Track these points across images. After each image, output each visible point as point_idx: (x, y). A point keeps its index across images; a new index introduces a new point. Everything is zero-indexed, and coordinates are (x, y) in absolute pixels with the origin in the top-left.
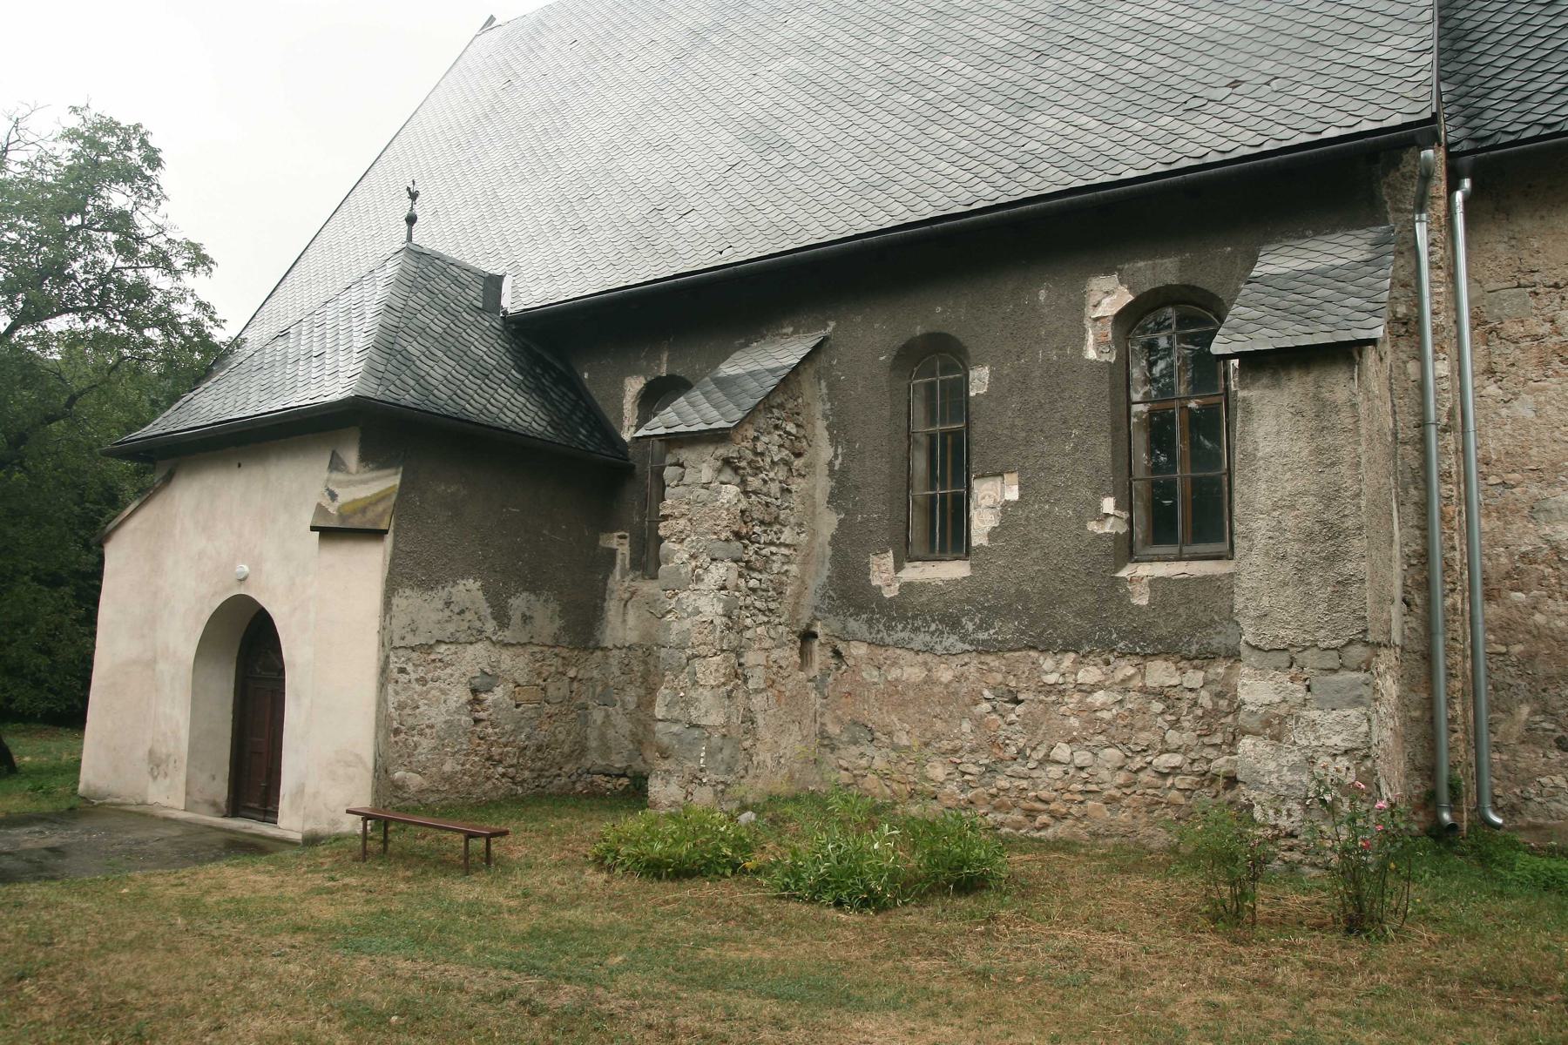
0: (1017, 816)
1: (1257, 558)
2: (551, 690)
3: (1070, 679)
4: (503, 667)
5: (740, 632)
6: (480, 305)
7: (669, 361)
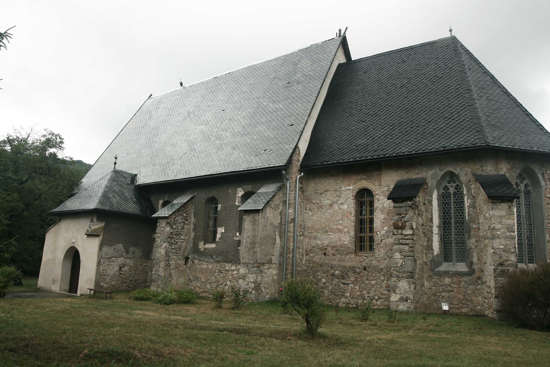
1: (243, 247)
4: (127, 263)
6: (129, 183)
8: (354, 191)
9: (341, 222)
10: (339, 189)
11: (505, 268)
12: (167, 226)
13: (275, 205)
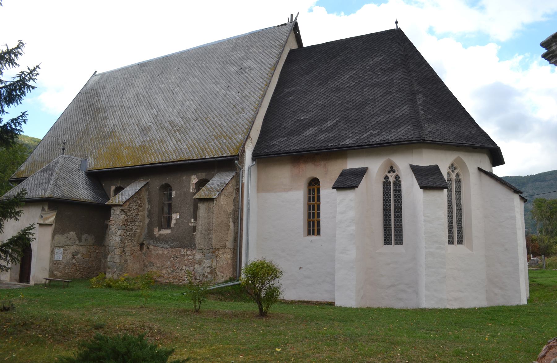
0: (177, 280)
2: (92, 255)
3: (186, 253)
7: (120, 183)
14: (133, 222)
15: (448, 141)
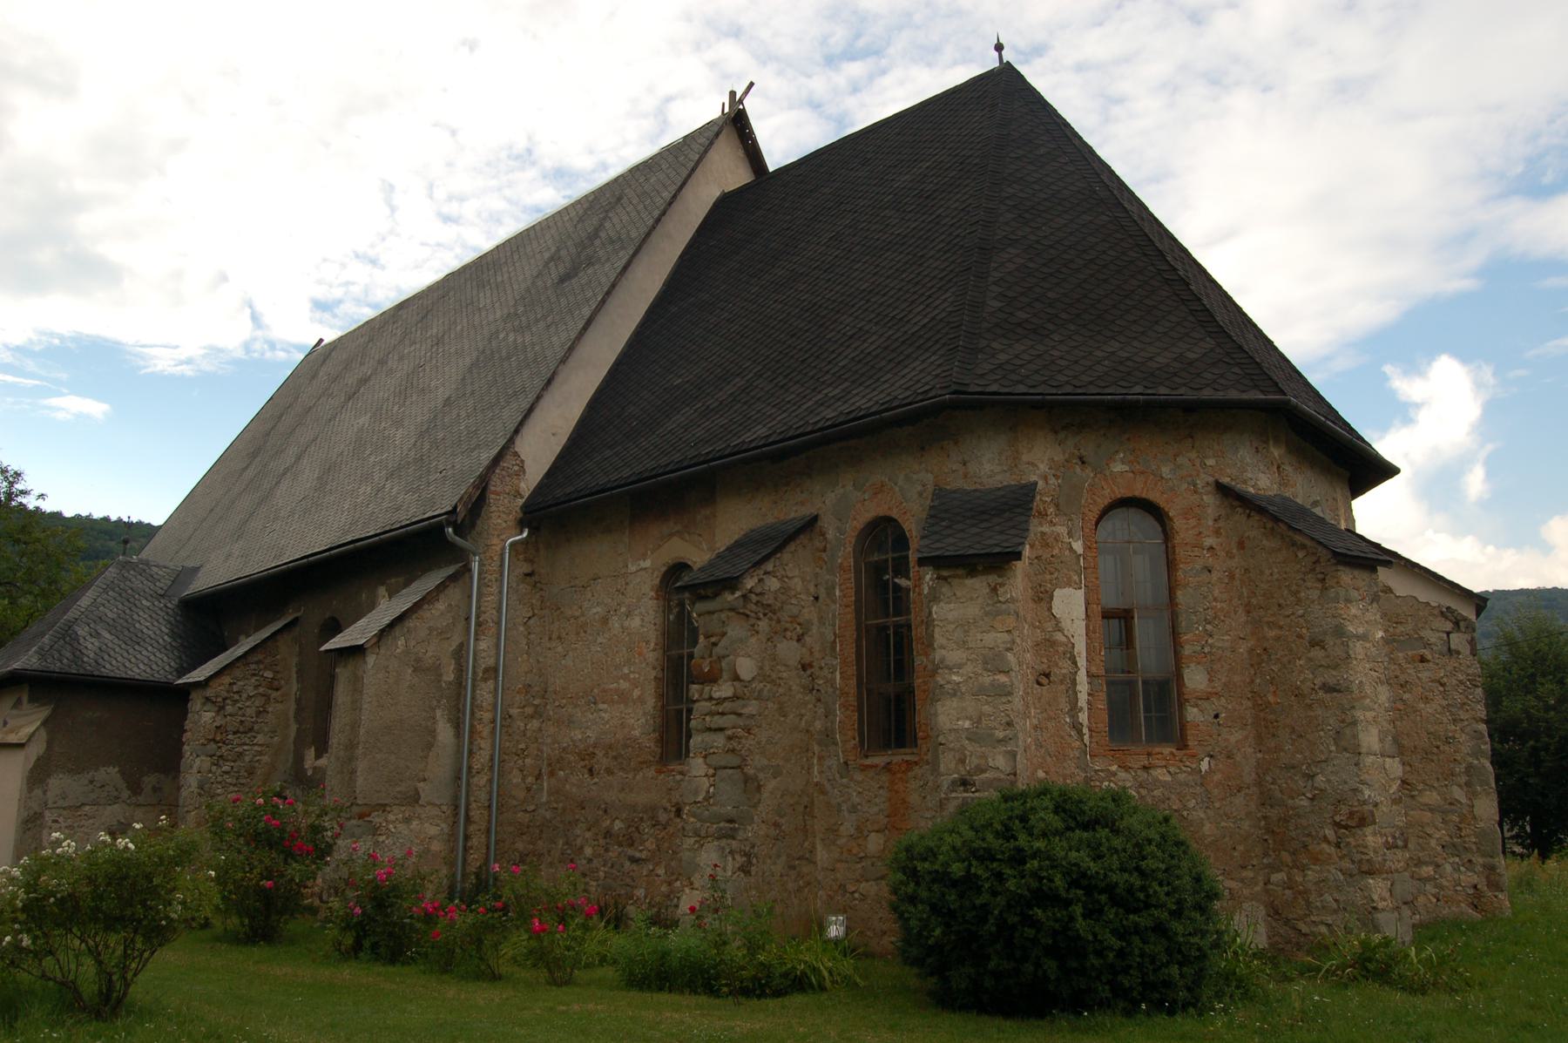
5: (212, 797)
8: (656, 573)
9: (626, 671)
10: (623, 571)
11: (977, 794)
12: (205, 708)
13: (430, 629)
14: (246, 733)
15: (1069, 389)
